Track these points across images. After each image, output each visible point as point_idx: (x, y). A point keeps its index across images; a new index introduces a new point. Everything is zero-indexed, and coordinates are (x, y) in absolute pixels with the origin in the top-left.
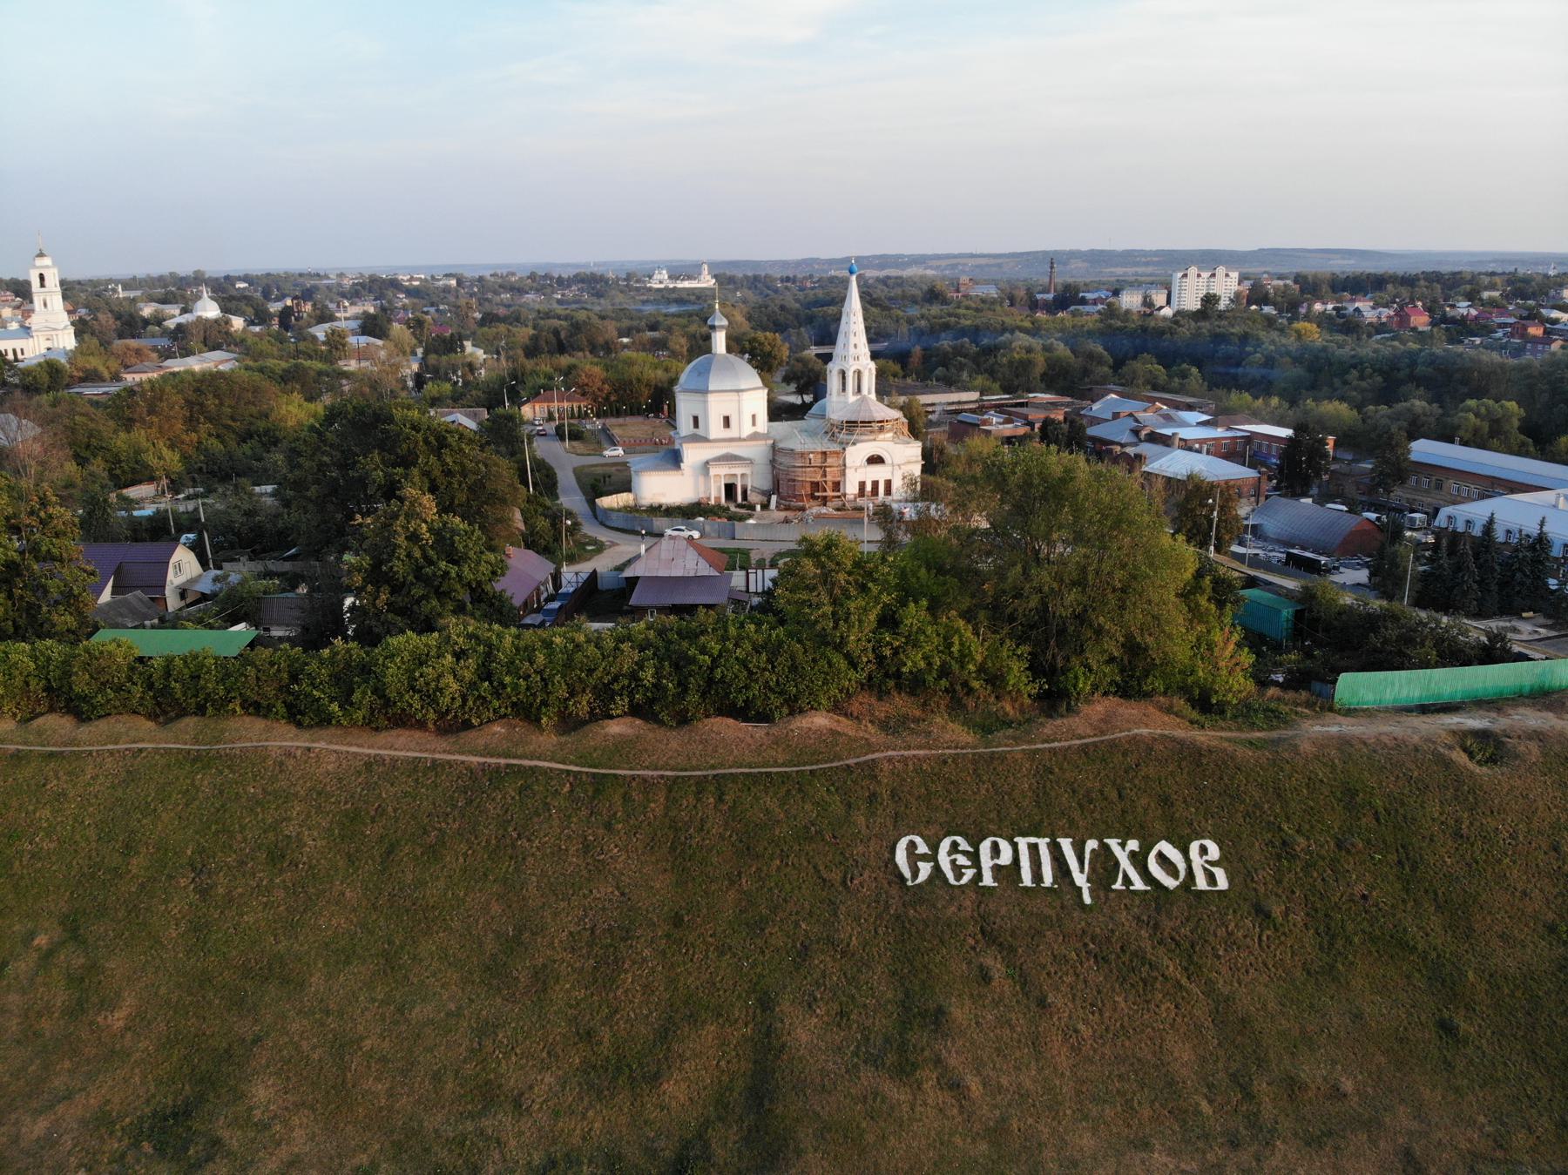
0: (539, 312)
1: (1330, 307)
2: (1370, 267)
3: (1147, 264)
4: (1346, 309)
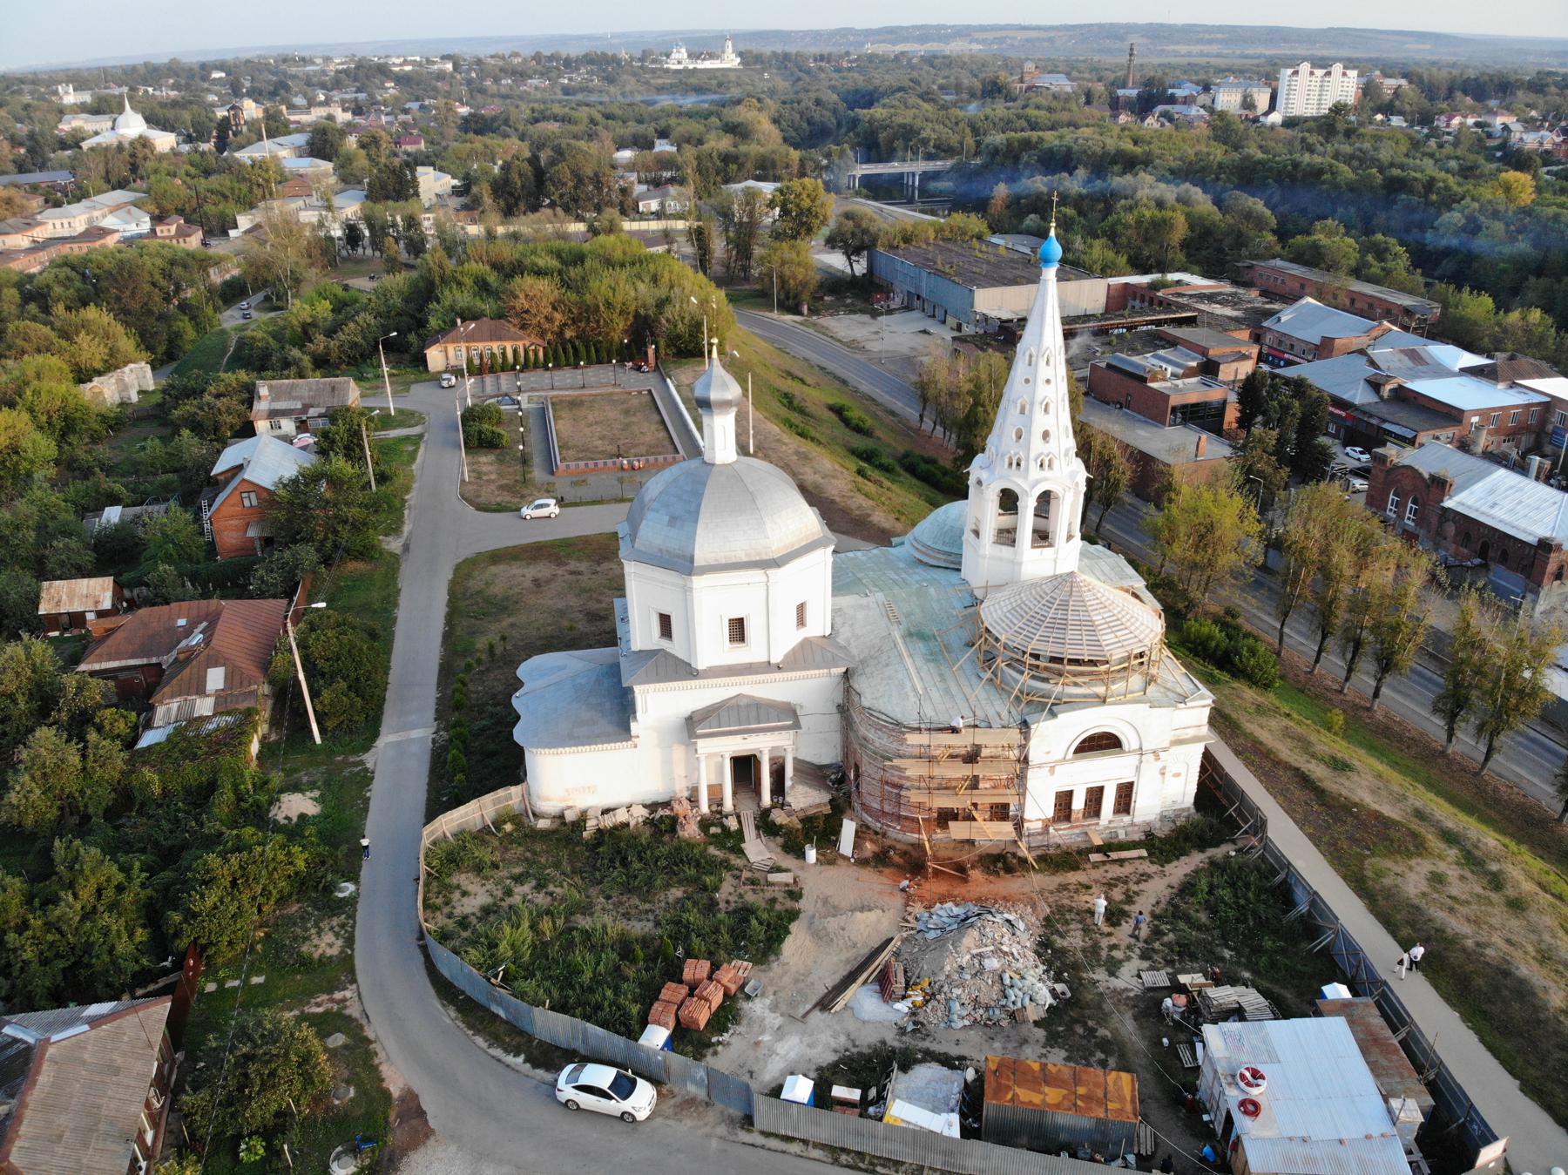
3: (1210, 42)
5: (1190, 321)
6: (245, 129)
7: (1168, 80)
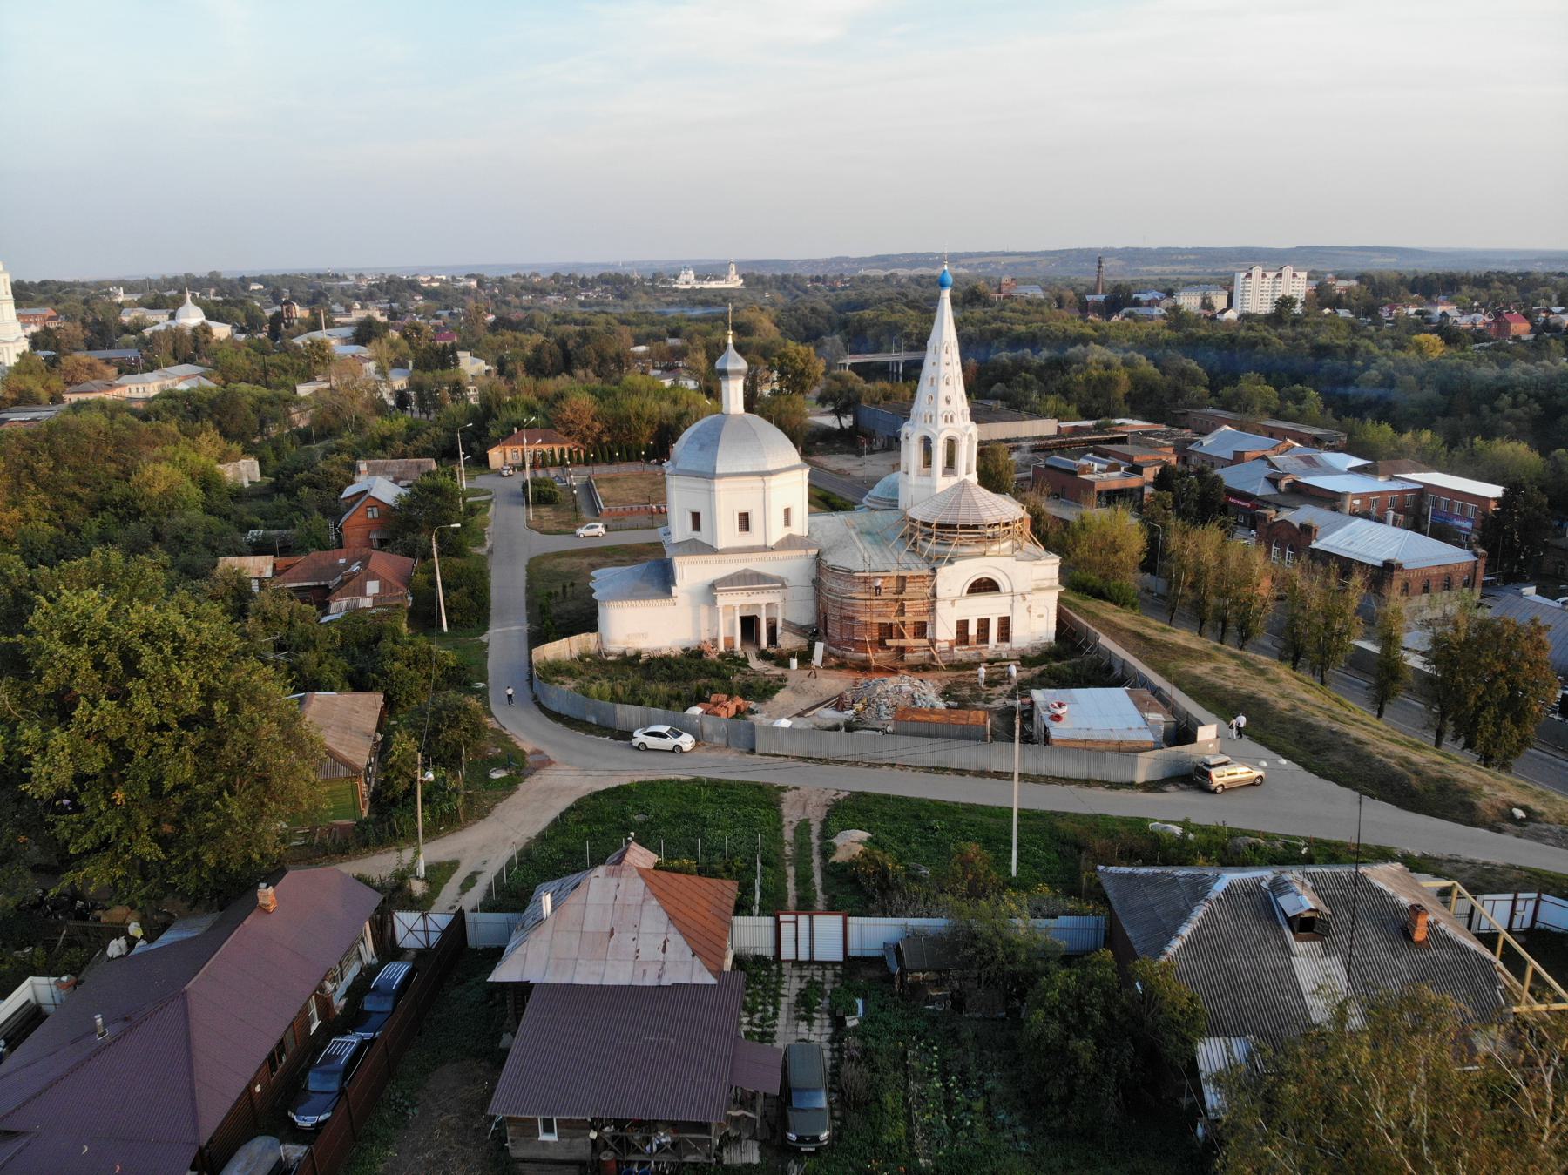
0: (555, 316)
1: (1412, 310)
2: (1426, 267)
3: (1183, 262)
4: (1430, 313)
5: (1122, 441)
6: (296, 322)
7: (1133, 289)
